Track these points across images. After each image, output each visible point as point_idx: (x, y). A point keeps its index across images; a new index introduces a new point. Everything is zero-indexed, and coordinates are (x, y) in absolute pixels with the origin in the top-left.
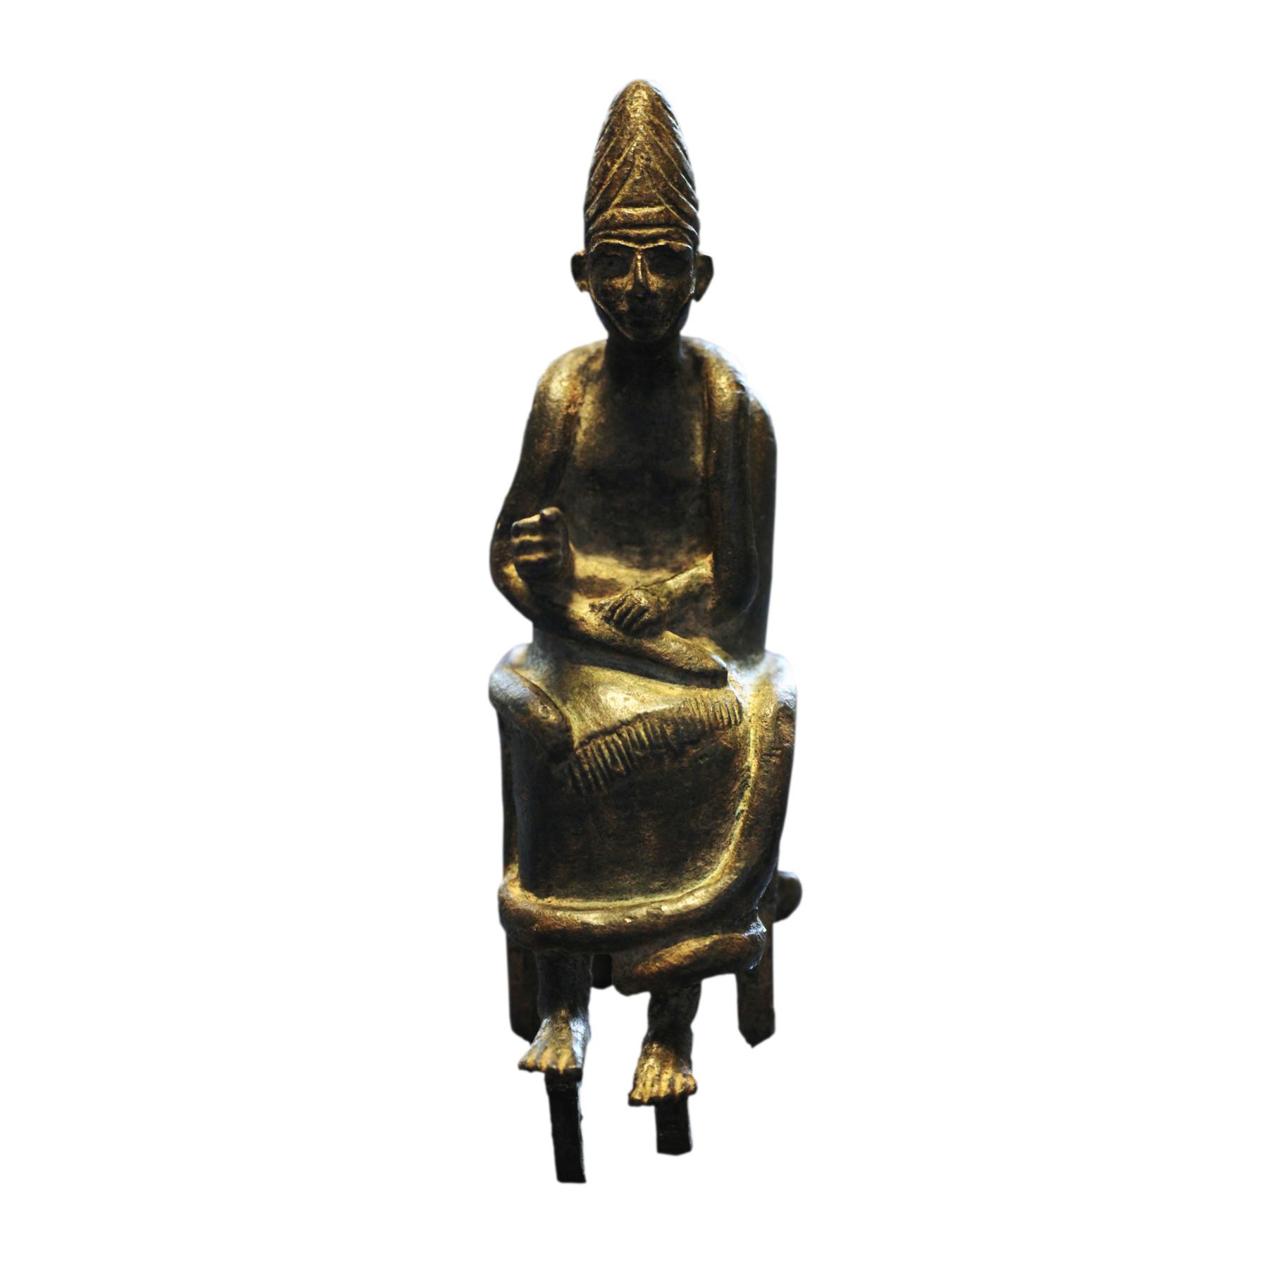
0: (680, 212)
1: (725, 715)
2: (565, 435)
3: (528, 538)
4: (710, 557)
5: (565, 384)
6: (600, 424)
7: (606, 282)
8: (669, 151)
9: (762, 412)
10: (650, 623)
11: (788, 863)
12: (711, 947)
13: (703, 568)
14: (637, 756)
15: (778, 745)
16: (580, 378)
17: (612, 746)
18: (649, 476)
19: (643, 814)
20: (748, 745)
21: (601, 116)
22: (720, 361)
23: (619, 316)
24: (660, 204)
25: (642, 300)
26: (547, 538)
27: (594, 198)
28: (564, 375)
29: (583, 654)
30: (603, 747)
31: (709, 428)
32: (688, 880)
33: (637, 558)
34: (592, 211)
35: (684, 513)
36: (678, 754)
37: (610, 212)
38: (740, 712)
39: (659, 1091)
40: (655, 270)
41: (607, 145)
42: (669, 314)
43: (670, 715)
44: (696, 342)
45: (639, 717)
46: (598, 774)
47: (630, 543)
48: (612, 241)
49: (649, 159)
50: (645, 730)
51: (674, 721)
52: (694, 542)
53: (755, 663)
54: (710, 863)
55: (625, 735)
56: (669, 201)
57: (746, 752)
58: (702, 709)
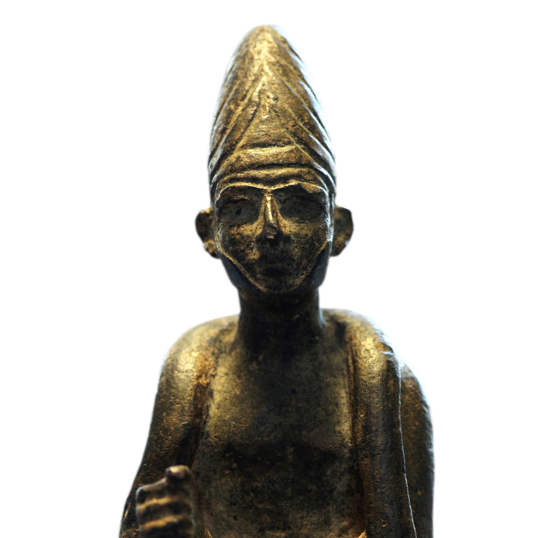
2: (196, 406)
3: (154, 501)
5: (195, 354)
6: (236, 396)
7: (234, 231)
8: (298, 92)
9: (413, 379)
16: (212, 349)
18: (292, 450)
21: (225, 62)
22: (365, 324)
23: (249, 266)
24: (289, 143)
25: (274, 243)
26: (176, 499)
27: (217, 145)
28: (194, 346)
31: (356, 402)
34: (215, 161)
35: (331, 491)
37: (235, 154)
40: (287, 213)
41: (230, 89)
42: (304, 262)
44: (332, 310)
48: (238, 184)
49: (276, 99)
52: (345, 523)
56: (300, 141)
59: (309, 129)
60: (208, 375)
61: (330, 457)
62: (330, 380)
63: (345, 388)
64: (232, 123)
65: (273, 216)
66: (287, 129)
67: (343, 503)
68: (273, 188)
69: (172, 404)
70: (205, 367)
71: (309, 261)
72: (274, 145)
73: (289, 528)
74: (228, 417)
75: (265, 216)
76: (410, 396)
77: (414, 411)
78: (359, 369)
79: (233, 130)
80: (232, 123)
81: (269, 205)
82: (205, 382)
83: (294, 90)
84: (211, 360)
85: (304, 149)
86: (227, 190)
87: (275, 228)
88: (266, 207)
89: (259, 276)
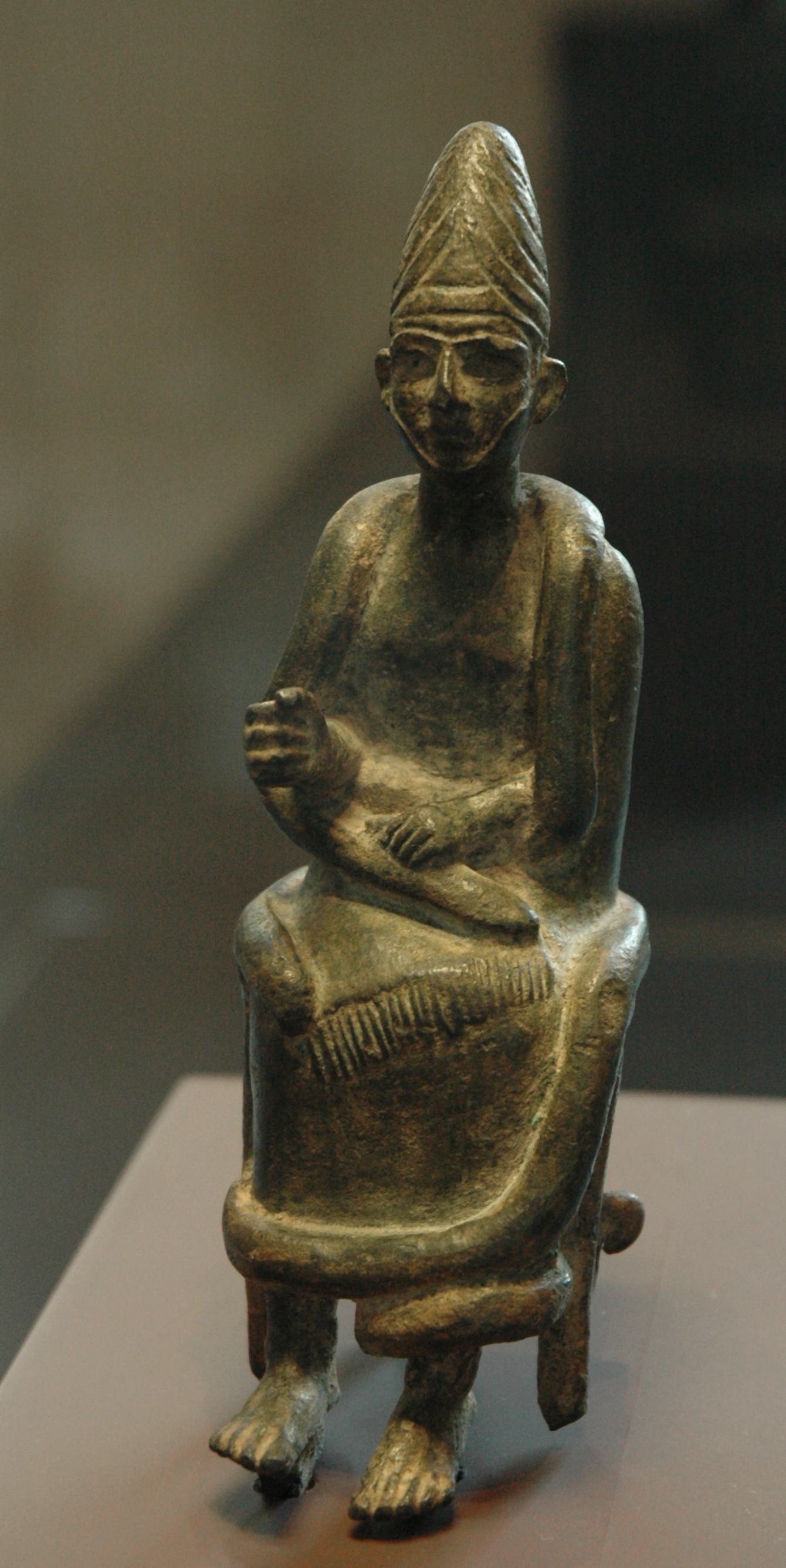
0: (513, 296)
1: (525, 985)
2: (350, 595)
4: (532, 770)
6: (402, 582)
10: (434, 853)
11: (619, 1180)
12: (480, 1305)
13: (522, 784)
14: (398, 1034)
15: (595, 1032)
17: (366, 1019)
18: (462, 655)
19: (404, 1114)
20: (556, 1029)
23: (419, 435)
24: (483, 283)
29: (354, 888)
30: (354, 1019)
32: (461, 1207)
33: (445, 764)
35: (505, 709)
36: (454, 1036)
38: (551, 982)
39: (393, 1498)
40: (467, 370)
43: (447, 982)
45: (404, 981)
46: (345, 1055)
47: (435, 743)
50: (412, 999)
51: (450, 990)
52: (521, 746)
53: (592, 914)
54: (494, 1187)
55: (384, 1004)
56: (497, 280)
57: (552, 1039)
58: (493, 975)
59: (512, 265)
60: (374, 554)
61: (505, 670)
62: (518, 573)
63: (534, 584)
64: (419, 250)
65: (448, 377)
66: (482, 264)
67: (519, 722)
68: (454, 341)
69: (323, 588)
70: (369, 545)
71: (493, 434)
72: (463, 284)
73: (454, 745)
74: (391, 607)
75: (441, 376)
76: (613, 600)
77: (616, 620)
78: (550, 567)
79: (418, 260)
80: (419, 250)
81: (446, 363)
82: (367, 563)
83: (500, 214)
84: (381, 534)
85: (501, 291)
86: (400, 336)
87: (447, 393)
88: (443, 364)
89: (430, 448)
